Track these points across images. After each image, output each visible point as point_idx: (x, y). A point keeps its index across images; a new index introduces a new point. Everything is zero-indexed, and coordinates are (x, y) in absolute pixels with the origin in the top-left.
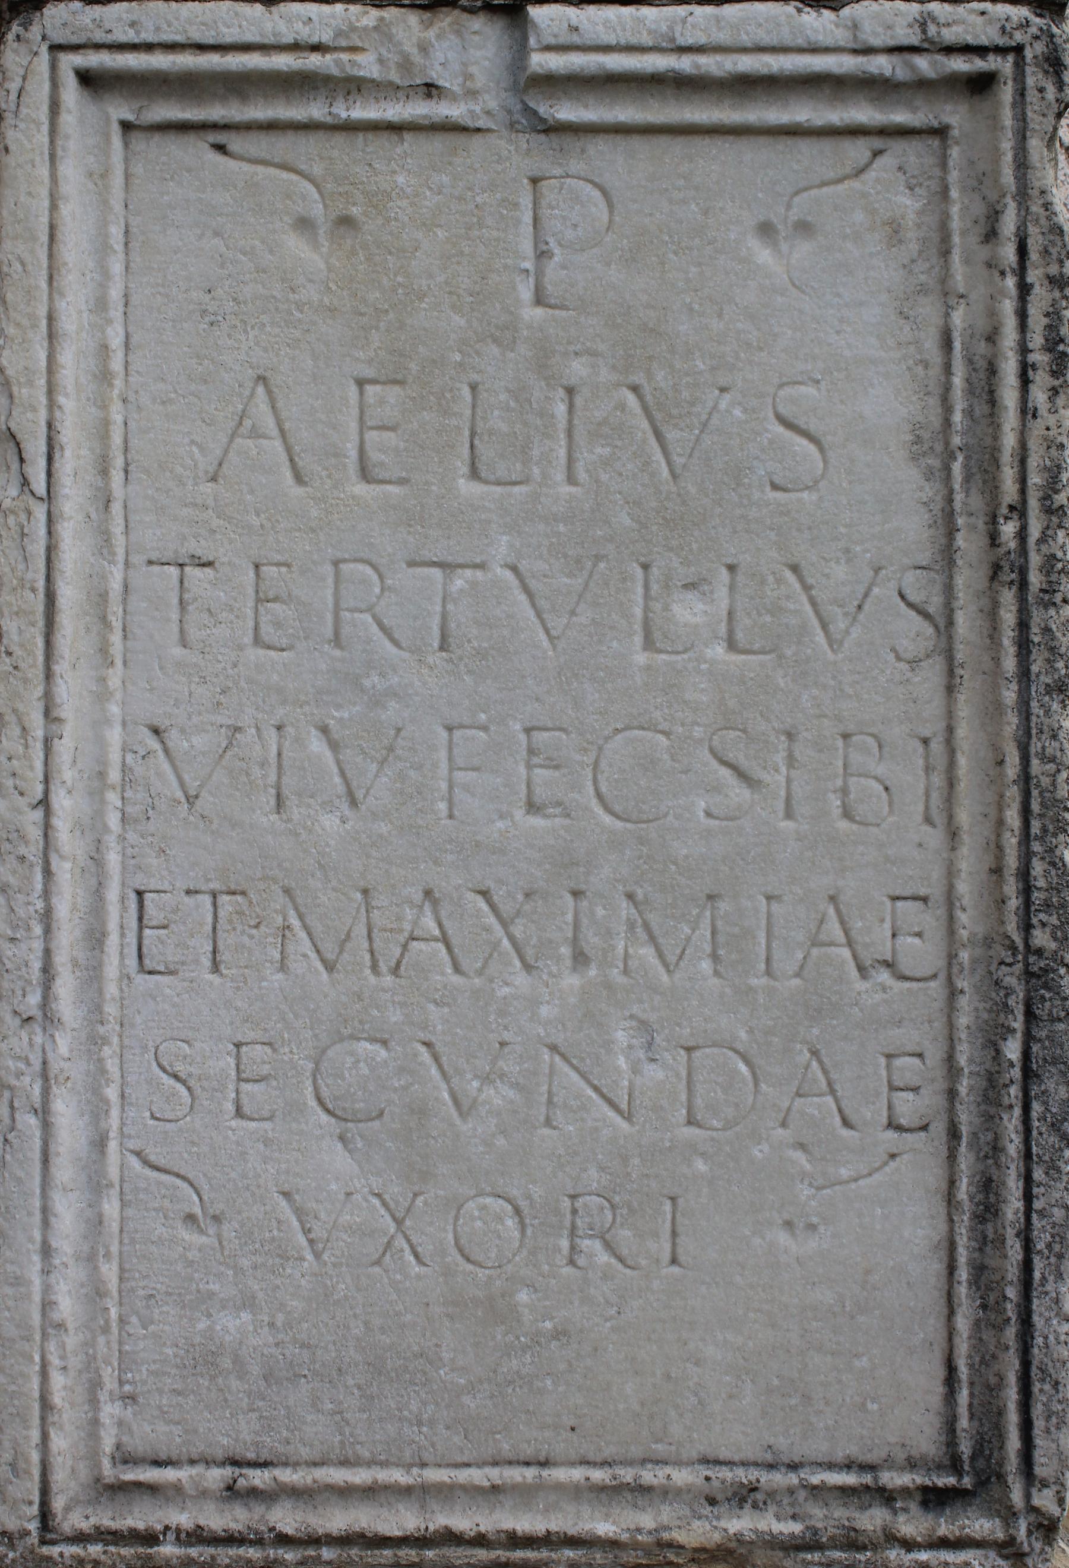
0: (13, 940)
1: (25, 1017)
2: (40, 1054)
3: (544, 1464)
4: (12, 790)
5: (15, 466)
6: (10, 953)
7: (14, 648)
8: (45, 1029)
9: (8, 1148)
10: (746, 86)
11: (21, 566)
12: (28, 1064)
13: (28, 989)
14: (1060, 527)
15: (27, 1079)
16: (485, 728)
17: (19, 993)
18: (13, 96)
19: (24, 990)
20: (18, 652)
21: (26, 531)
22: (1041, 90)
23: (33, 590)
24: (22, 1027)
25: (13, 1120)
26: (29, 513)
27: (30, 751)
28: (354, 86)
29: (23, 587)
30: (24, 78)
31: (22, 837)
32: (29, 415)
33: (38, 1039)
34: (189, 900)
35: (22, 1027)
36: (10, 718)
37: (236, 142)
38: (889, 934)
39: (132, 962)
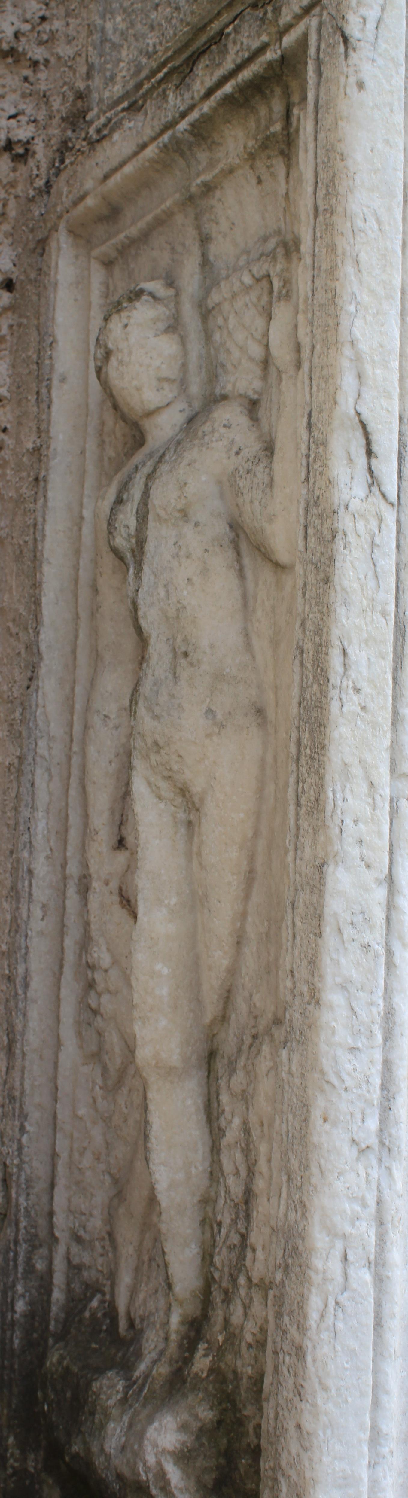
0: (353, 1050)
1: (363, 1146)
2: (376, 1192)
4: (358, 861)
5: (361, 460)
6: (349, 1067)
7: (363, 684)
8: (380, 1160)
9: (339, 1313)
11: (371, 583)
12: (364, 1206)
13: (368, 1111)
15: (363, 1225)
17: (359, 1116)
18: (371, 25)
19: (363, 1114)
20: (367, 689)
21: (377, 541)
23: (384, 614)
24: (358, 1159)
25: (346, 1276)
26: (381, 520)
27: (378, 812)
29: (373, 609)
30: (383, 9)
31: (367, 921)
32: (383, 402)
33: (375, 1174)
35: (358, 1159)
36: (357, 771)
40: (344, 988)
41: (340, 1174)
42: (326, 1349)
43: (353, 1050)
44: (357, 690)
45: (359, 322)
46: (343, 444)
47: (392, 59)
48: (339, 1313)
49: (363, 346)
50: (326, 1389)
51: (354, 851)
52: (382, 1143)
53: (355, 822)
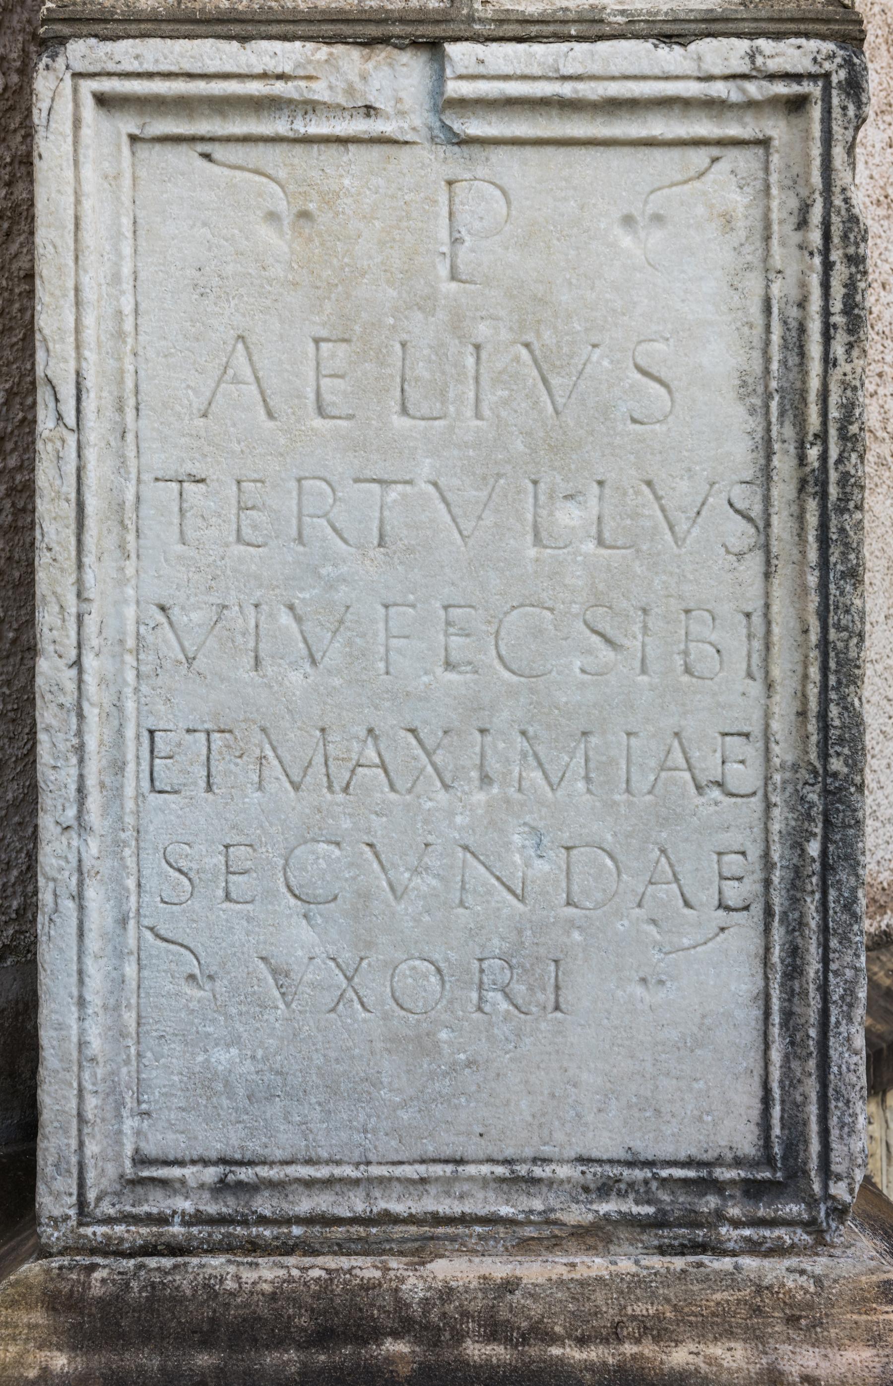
0: (54, 767)
3: (460, 1162)
4: (53, 654)
6: (53, 778)
9: (52, 925)
10: (614, 106)
12: (68, 862)
13: (67, 805)
14: (853, 450)
16: (413, 606)
17: (60, 808)
21: (61, 455)
22: (844, 108)
24: (62, 834)
25: (56, 904)
26: (63, 441)
28: (310, 107)
33: (75, 843)
34: (189, 738)
35: (62, 834)
36: (51, 598)
37: (219, 151)
38: (720, 761)
39: (146, 784)
40: (47, 730)
41: (49, 842)
42: (44, 946)
43: (54, 767)
44: (50, 550)
45: (43, 316)
46: (43, 395)
47: (61, 134)
48: (52, 925)
49: (46, 332)
50: (45, 970)
51: (51, 648)
52: (80, 825)
53: (51, 630)
